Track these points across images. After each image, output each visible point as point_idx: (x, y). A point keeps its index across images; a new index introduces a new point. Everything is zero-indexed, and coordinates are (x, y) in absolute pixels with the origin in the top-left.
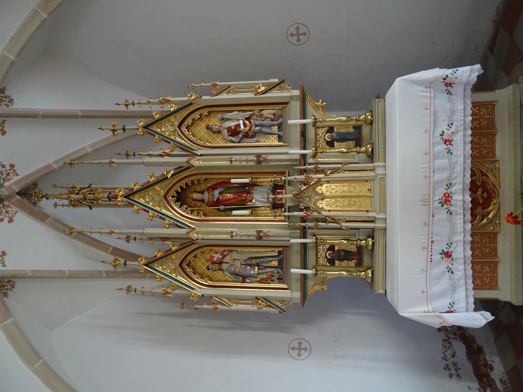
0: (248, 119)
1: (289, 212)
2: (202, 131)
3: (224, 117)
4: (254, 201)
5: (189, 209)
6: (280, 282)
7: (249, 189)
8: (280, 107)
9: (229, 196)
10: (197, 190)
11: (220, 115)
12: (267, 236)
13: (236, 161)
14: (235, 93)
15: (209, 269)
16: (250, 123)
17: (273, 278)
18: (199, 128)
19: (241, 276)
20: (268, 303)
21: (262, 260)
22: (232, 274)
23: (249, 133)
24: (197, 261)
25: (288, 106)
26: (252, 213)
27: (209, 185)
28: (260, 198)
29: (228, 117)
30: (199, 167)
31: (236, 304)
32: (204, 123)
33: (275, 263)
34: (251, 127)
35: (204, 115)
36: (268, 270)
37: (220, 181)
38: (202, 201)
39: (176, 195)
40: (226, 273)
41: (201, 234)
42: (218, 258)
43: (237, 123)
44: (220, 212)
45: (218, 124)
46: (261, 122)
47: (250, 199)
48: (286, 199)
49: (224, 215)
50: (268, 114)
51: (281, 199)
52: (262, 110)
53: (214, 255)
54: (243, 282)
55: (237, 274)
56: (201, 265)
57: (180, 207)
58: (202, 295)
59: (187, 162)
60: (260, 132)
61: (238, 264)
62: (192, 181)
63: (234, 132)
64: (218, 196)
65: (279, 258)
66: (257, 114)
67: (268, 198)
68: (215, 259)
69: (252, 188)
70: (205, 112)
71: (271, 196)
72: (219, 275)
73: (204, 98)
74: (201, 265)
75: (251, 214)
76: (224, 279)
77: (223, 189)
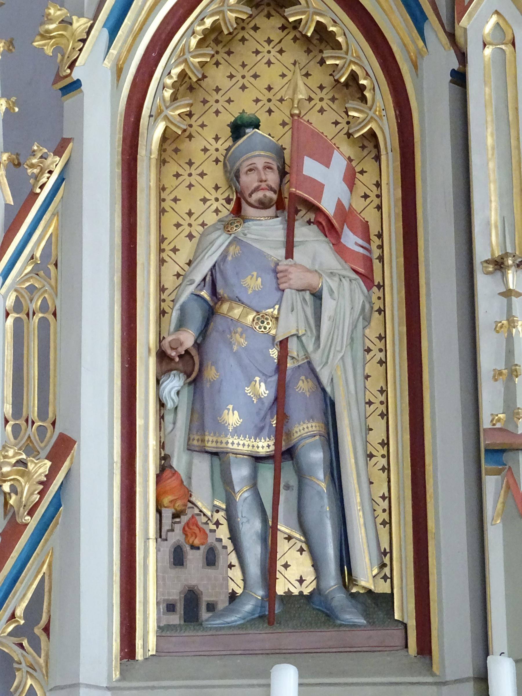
6: (171, 608)
15: (238, 129)
17: (194, 558)
19: (198, 345)
20: (32, 523)
21: (320, 479)
22: (212, 281)
24: (288, 58)
31: (18, 306)
33: (292, 574)
36: (251, 528)
40: (221, 241)
42: (318, 188)
53: (339, 163)
54: (162, 356)
55: (211, 313)
56: (262, 83)
58: (76, 85)
61: (291, 321)
65: (339, 598)
68: (311, 168)
72: (202, 199)
74: (262, 83)
76: (170, 232)
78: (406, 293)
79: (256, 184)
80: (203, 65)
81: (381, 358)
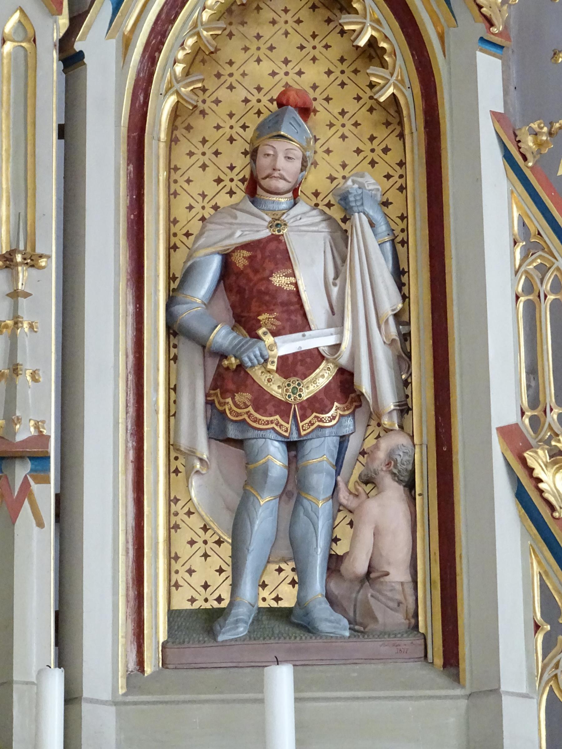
0: (345, 381)
2: (266, 66)
3: (360, 221)
8: (430, 622)
11: (372, 183)
14: (529, 288)
16: (317, 404)
18: (287, 47)
23: (243, 397)
25: (432, 675)
29: (356, 243)
32: (323, 80)
34: (282, 408)
35: (376, 74)
43: (315, 304)
45: (315, 180)
46: (320, 481)
50: (376, 534)
52: (410, 486)
60: (253, 476)
63: (252, 287)
66: (381, 455)
70: (395, 81)
73: (489, 71)
78: (429, 231)
79: (269, 171)
80: (215, 37)
81: (403, 238)
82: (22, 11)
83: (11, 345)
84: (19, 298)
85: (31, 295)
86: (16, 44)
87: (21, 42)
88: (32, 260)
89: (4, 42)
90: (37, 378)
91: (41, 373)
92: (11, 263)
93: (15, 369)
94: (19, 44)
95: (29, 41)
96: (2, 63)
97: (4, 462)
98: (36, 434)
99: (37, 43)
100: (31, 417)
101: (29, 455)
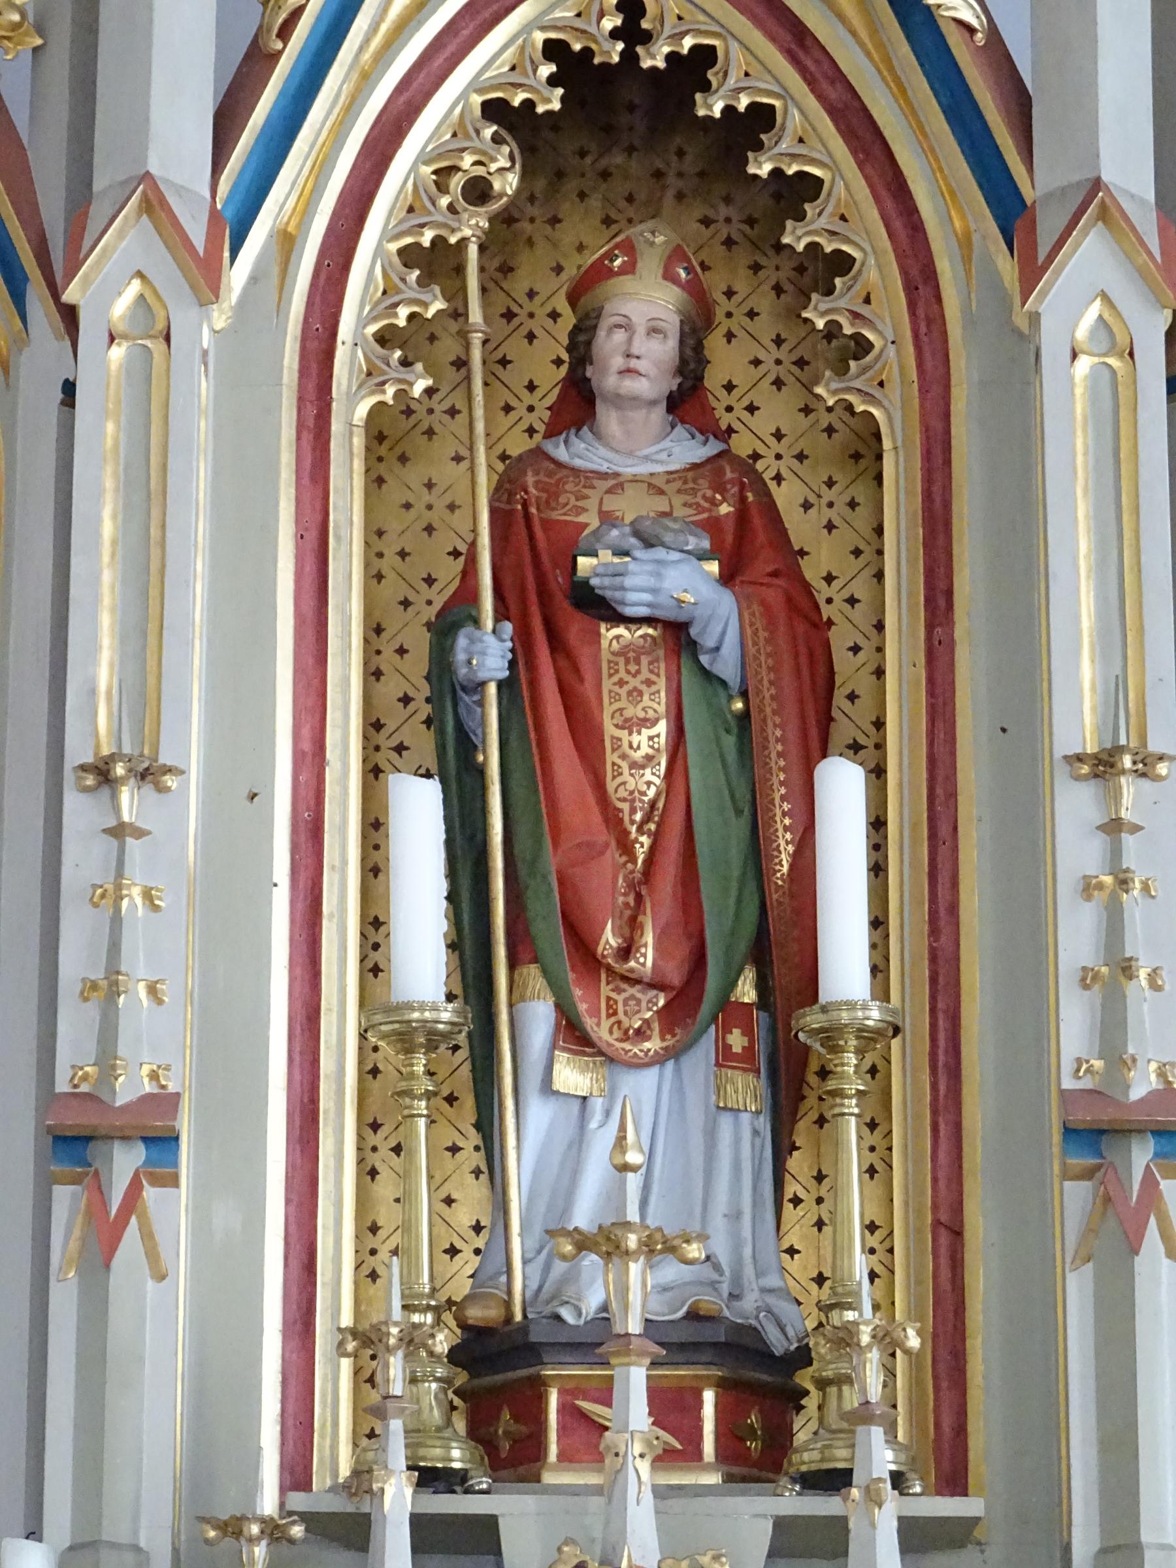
1: (418, 1522)
4: (571, 1076)
5: (472, 225)
7: (729, 1012)
9: (640, 750)
10: (715, 343)
12: (104, 1234)
13: (1114, 827)
26: (405, 1040)
27: (786, 497)
28: (620, 1160)
30: (1019, 355)
37: (840, 639)
38: (578, 403)
39: (654, 58)
41: (142, 373)
44: (420, 643)
47: (602, 1031)
48: (612, 1493)
49: (391, 687)
51: (589, 1436)
57: (494, 110)
59: (1092, 199)
62: (842, 263)
64: (636, 602)
67: (605, 1242)
69: (748, 1058)
71: (638, 1294)
75: (391, 1031)
77: (727, 666)
82: (1104, 296)
83: (1109, 918)
84: (1123, 835)
85: (1142, 828)
86: (1096, 360)
87: (1105, 355)
88: (1145, 765)
89: (1074, 356)
90: (1160, 983)
91: (1164, 973)
92: (1109, 770)
93: (1127, 969)
94: (1102, 360)
95: (1120, 356)
96: (1073, 394)
97: (1104, 1137)
98: (1161, 1087)
99: (1136, 357)
100: (1150, 1056)
101: (1153, 1128)
